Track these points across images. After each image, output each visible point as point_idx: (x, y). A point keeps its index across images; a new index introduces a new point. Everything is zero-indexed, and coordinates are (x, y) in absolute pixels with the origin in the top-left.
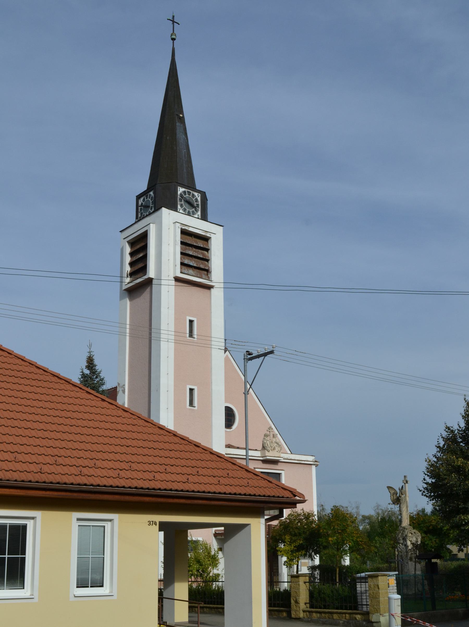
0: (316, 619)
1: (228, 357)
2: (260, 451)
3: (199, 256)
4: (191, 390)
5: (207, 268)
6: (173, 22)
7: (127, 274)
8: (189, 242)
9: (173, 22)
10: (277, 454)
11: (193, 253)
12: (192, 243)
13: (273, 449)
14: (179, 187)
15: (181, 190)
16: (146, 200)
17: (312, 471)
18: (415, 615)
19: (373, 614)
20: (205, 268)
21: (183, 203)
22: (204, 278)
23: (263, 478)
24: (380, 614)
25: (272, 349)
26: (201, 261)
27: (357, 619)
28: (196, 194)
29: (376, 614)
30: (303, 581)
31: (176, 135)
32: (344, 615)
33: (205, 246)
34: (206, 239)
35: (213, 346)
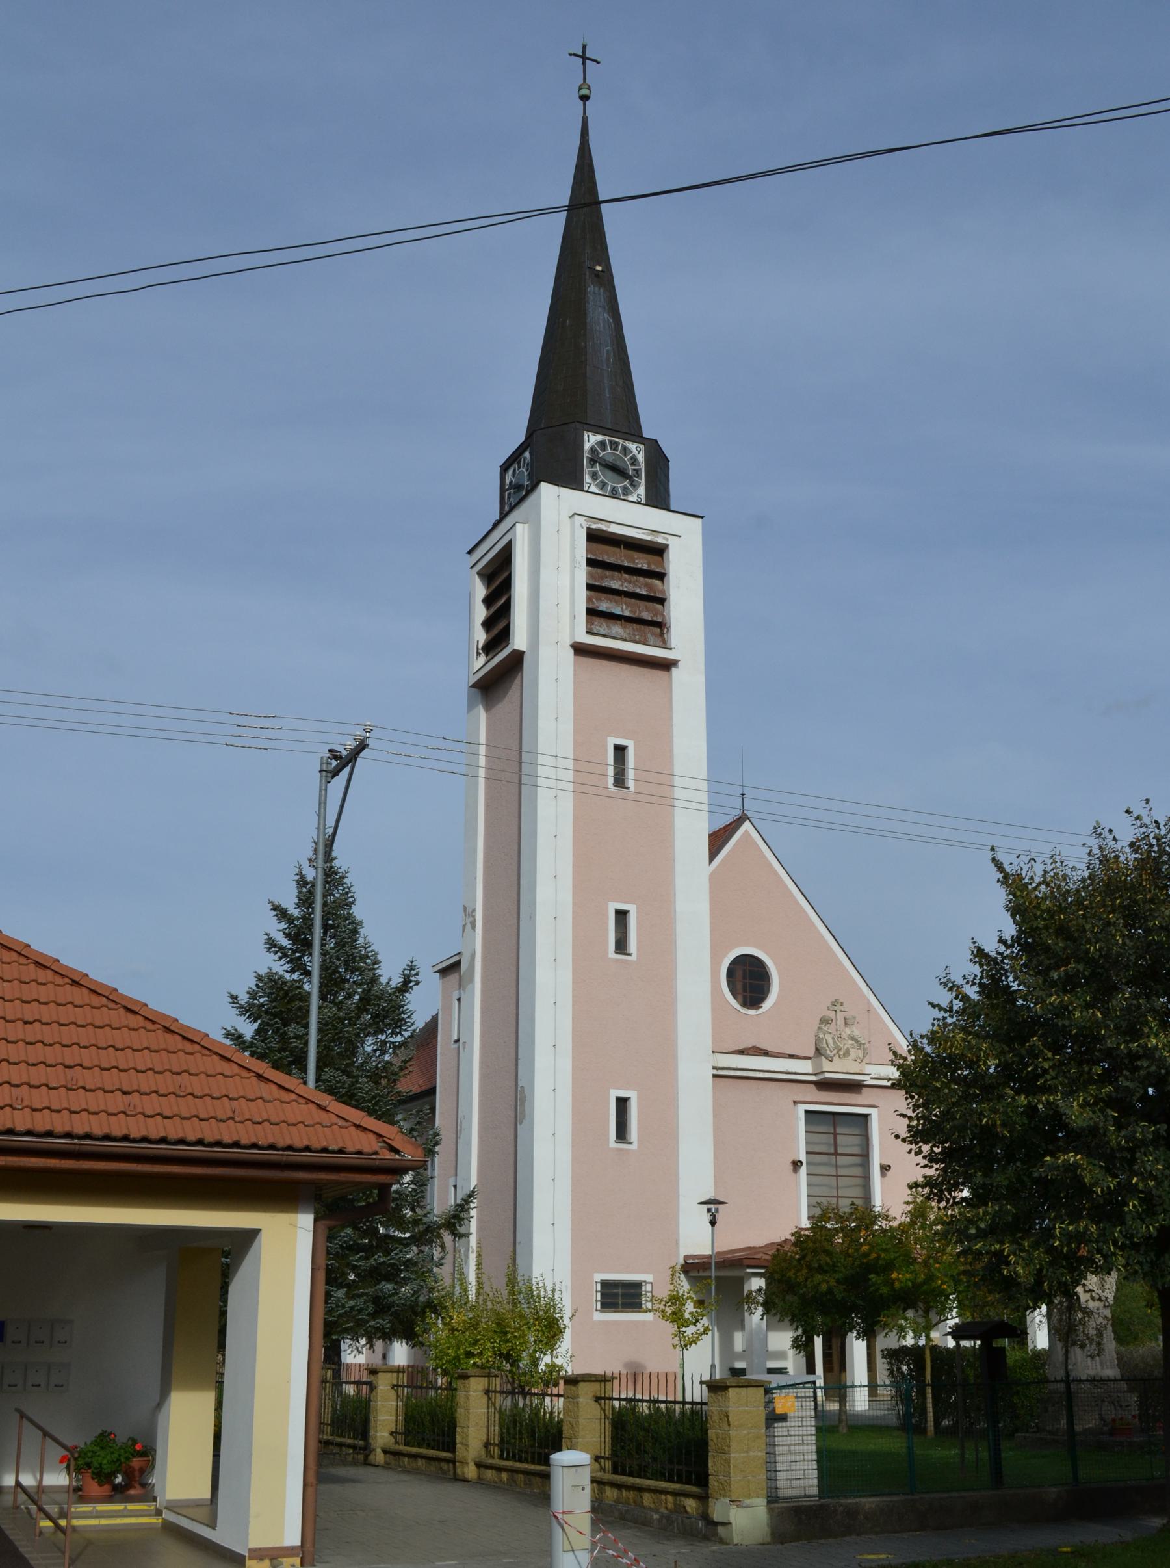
0: (610, 1502)
1: (749, 835)
2: (809, 1061)
3: (638, 590)
5: (659, 620)
6: (584, 58)
7: (478, 649)
8: (612, 560)
9: (584, 58)
10: (855, 1067)
11: (622, 585)
12: (620, 563)
13: (844, 1054)
14: (586, 434)
15: (591, 440)
16: (517, 472)
18: (867, 1506)
19: (717, 1499)
20: (655, 619)
21: (597, 468)
22: (651, 643)
23: (304, 1098)
24: (732, 1501)
25: (364, 734)
26: (643, 604)
27: (689, 1509)
28: (632, 446)
29: (722, 1499)
30: (591, 1395)
31: (585, 314)
32: (663, 1497)
33: (653, 568)
34: (658, 551)
35: (677, 803)
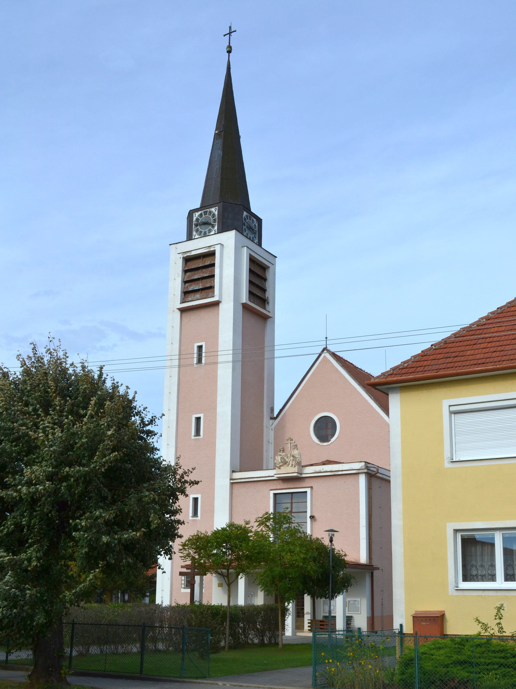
3: (205, 275)
4: (198, 419)
17: (358, 482)
